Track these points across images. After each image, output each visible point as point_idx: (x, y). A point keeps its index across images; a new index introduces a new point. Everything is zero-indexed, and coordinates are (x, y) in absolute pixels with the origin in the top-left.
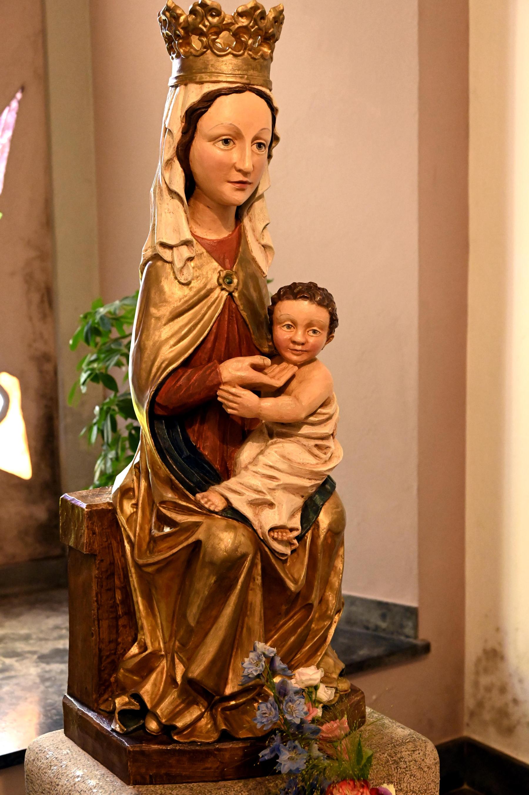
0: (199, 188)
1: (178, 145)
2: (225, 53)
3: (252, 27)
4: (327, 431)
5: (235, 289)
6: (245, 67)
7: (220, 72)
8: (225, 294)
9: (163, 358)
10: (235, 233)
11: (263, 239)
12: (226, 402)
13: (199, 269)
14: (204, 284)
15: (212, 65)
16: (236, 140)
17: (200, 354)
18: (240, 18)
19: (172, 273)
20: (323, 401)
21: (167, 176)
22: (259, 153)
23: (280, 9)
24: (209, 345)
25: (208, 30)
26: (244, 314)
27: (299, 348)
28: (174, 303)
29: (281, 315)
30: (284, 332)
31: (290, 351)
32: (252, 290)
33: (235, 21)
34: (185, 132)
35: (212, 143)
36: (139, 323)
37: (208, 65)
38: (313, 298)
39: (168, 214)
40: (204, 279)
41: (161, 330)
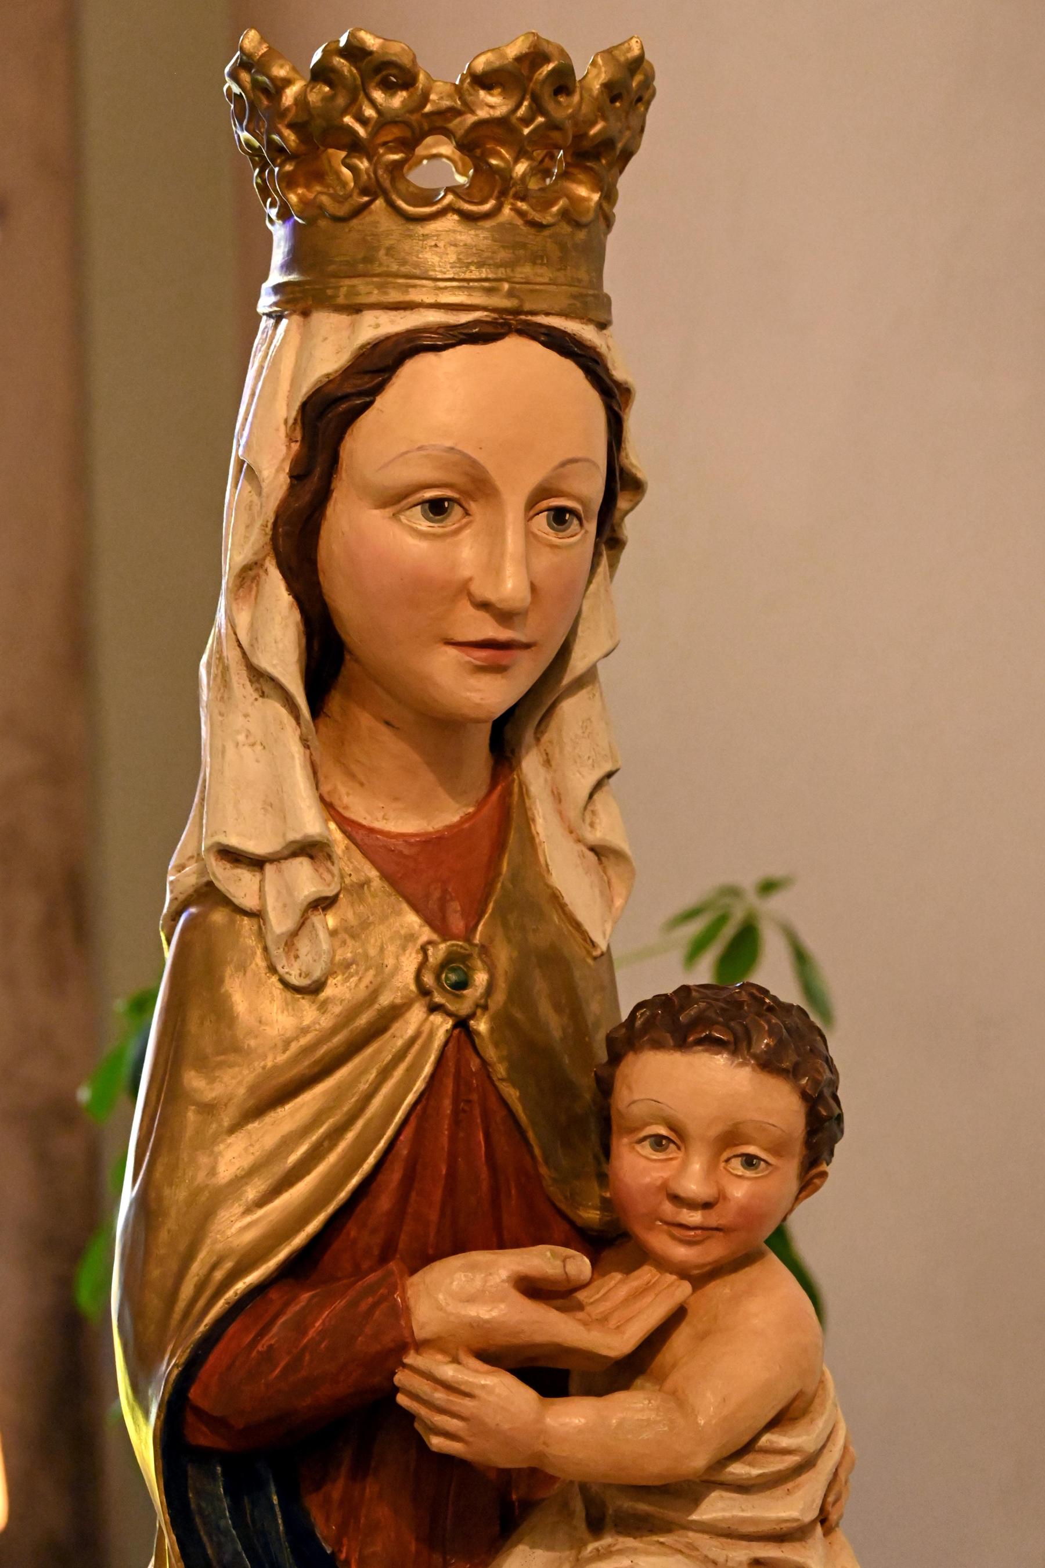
0: (357, 660)
1: (278, 516)
2: (434, 208)
3: (526, 121)
4: (794, 1514)
5: (477, 1006)
6: (503, 255)
7: (417, 272)
8: (443, 1025)
9: (219, 1246)
10: (486, 810)
11: (592, 825)
12: (422, 1411)
13: (354, 936)
14: (372, 988)
15: (390, 251)
16: (474, 500)
17: (352, 1230)
18: (482, 93)
19: (259, 952)
20: (779, 1408)
21: (243, 620)
22: (558, 541)
23: (629, 55)
24: (384, 1202)
25: (374, 134)
26: (511, 1093)
27: (695, 1217)
28: (265, 1057)
29: (634, 1102)
30: (643, 1163)
31: (665, 1227)
32: (545, 1009)
33: (465, 103)
34: (298, 475)
35: (389, 511)
36: (147, 1119)
37: (376, 249)
38: (745, 1044)
39: (247, 750)
40: (372, 972)
41: (216, 1149)
